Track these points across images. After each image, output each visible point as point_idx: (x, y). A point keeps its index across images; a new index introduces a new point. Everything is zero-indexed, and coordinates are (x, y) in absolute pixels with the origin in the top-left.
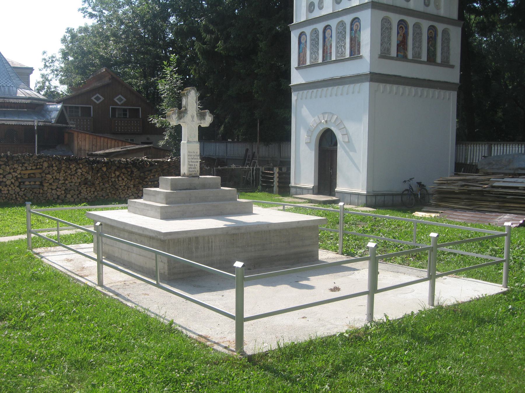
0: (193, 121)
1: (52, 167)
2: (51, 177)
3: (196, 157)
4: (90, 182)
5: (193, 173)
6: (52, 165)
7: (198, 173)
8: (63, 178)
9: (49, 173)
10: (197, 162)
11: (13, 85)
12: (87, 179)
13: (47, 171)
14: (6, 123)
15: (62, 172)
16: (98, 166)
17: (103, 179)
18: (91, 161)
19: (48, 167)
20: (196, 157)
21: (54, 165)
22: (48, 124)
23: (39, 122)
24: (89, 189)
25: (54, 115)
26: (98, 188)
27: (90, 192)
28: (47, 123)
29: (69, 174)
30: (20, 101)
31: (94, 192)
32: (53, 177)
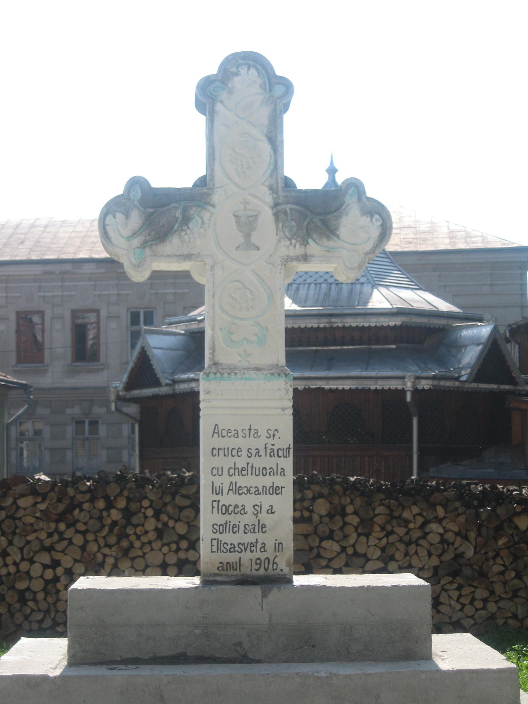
0: (249, 245)
1: (343, 514)
2: (337, 548)
3: (269, 462)
4: (471, 566)
5: (246, 556)
6: (343, 508)
7: (283, 562)
8: (378, 553)
9: (330, 536)
10: (277, 490)
11: (363, 280)
12: (461, 555)
13: (323, 529)
14: (327, 387)
15: (377, 532)
16: (499, 511)
17: (516, 558)
18: (474, 496)
19: (331, 516)
20: (269, 462)
21: (350, 509)
22: (448, 384)
23: (418, 378)
24: (466, 591)
25: (470, 356)
26: (498, 589)
27: (471, 603)
28: (442, 383)
29: (401, 540)
30: (373, 322)
31: (485, 601)
32: (343, 549)
